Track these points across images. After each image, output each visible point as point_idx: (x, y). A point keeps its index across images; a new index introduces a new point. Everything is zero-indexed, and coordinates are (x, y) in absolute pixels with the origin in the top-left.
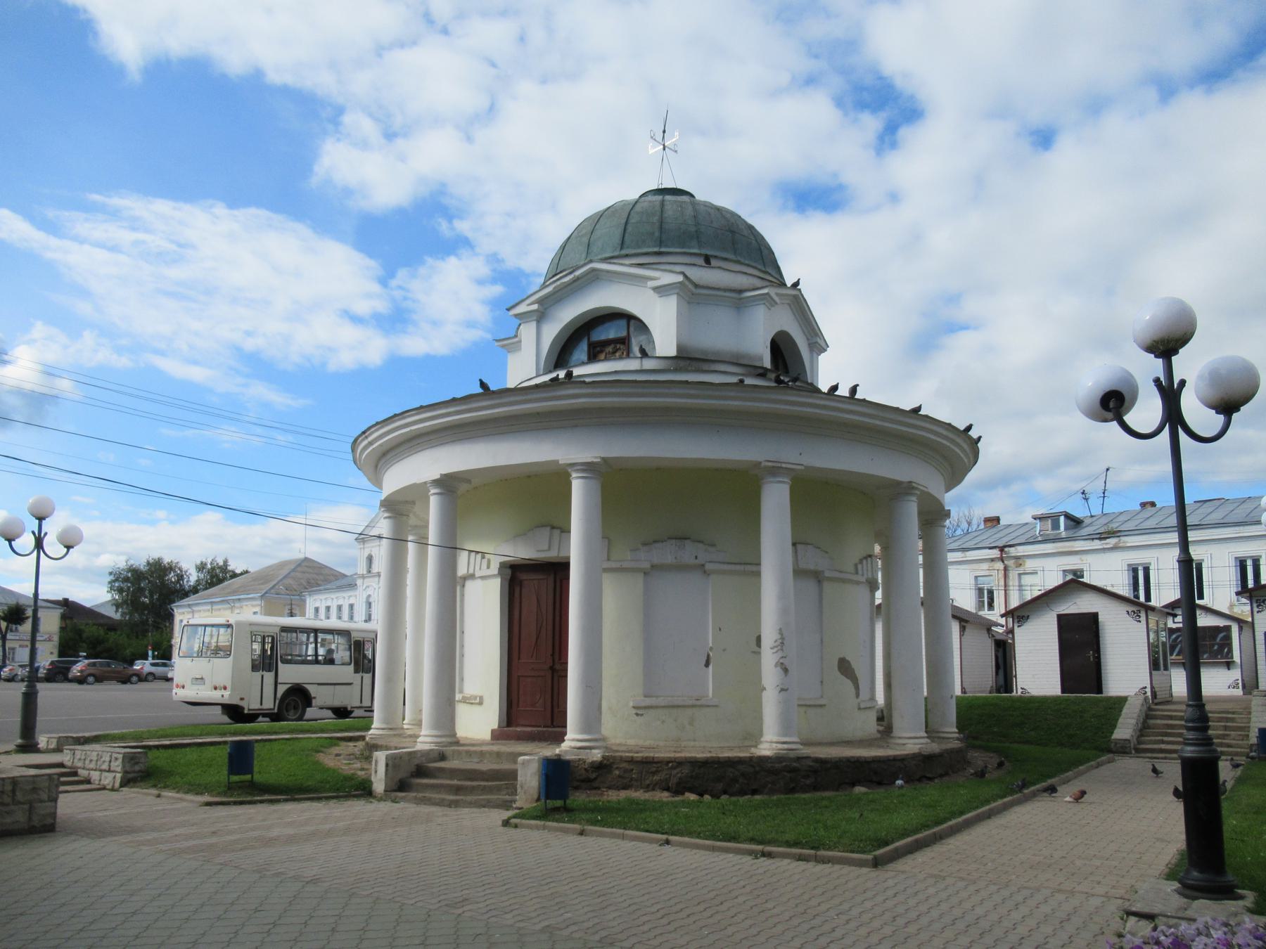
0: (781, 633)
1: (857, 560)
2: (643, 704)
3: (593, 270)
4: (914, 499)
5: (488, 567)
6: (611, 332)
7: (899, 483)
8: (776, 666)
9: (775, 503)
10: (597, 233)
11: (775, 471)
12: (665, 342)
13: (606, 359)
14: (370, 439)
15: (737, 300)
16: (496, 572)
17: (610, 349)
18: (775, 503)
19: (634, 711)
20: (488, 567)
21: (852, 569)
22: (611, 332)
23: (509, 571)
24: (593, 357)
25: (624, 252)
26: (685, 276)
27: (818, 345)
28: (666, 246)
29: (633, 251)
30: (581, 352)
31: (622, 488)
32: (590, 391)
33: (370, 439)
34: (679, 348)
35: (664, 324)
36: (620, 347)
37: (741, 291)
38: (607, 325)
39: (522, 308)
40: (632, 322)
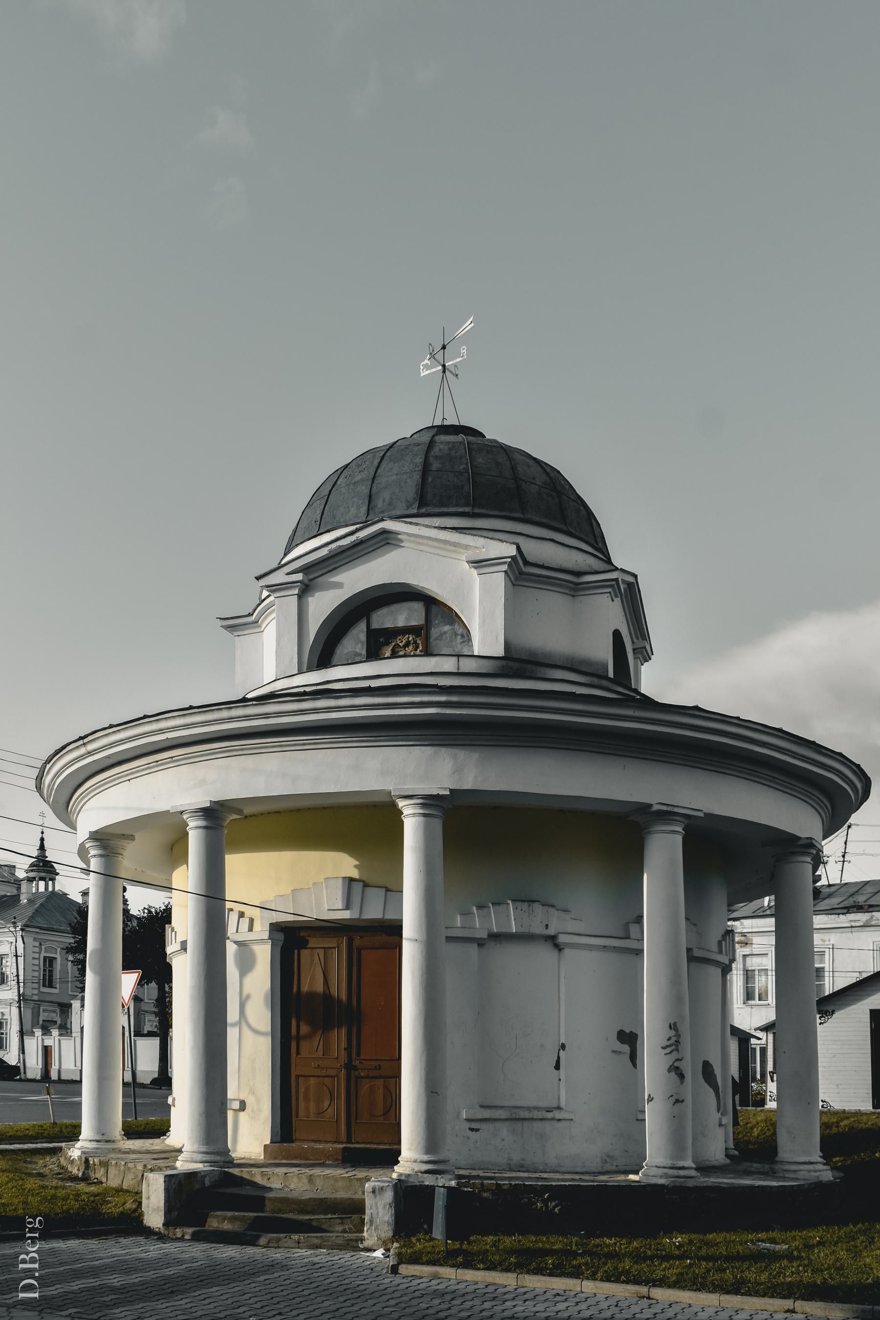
0: (673, 1027)
1: (719, 938)
2: (480, 1116)
3: (384, 532)
4: (809, 859)
5: (251, 929)
6: (404, 616)
7: (796, 838)
8: (669, 1071)
9: (664, 852)
10: (382, 481)
11: (666, 816)
12: (486, 635)
13: (394, 655)
14: (90, 747)
15: (573, 584)
16: (266, 935)
17: (401, 641)
18: (664, 852)
19: (467, 1125)
20: (251, 929)
21: (715, 948)
22: (404, 616)
23: (281, 936)
24: (373, 654)
25: (423, 510)
26: (519, 548)
27: (644, 654)
28: (481, 506)
29: (436, 510)
30: (356, 639)
31: (470, 828)
32: (443, 698)
33: (90, 747)
34: (507, 646)
35: (484, 614)
36: (420, 638)
37: (579, 574)
38: (394, 607)
39: (279, 577)
40: (434, 609)
